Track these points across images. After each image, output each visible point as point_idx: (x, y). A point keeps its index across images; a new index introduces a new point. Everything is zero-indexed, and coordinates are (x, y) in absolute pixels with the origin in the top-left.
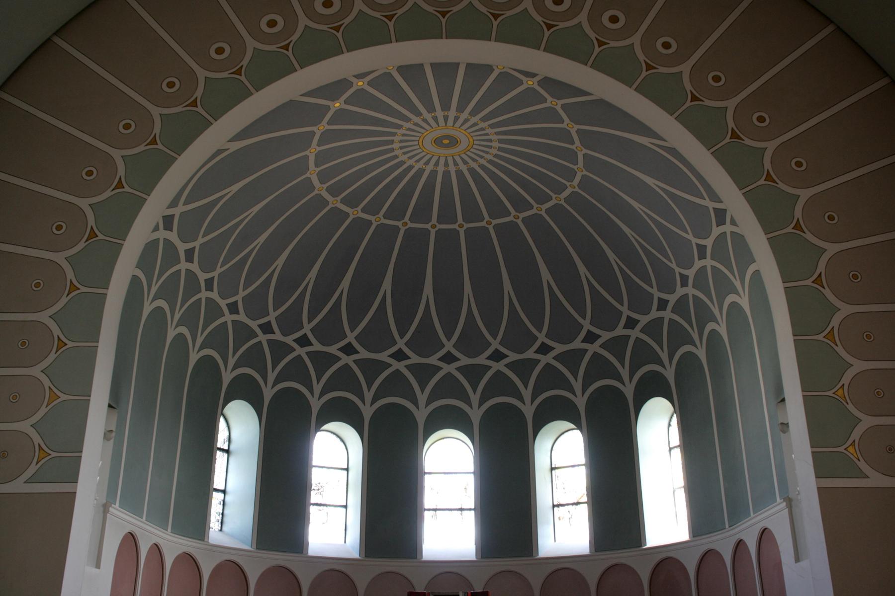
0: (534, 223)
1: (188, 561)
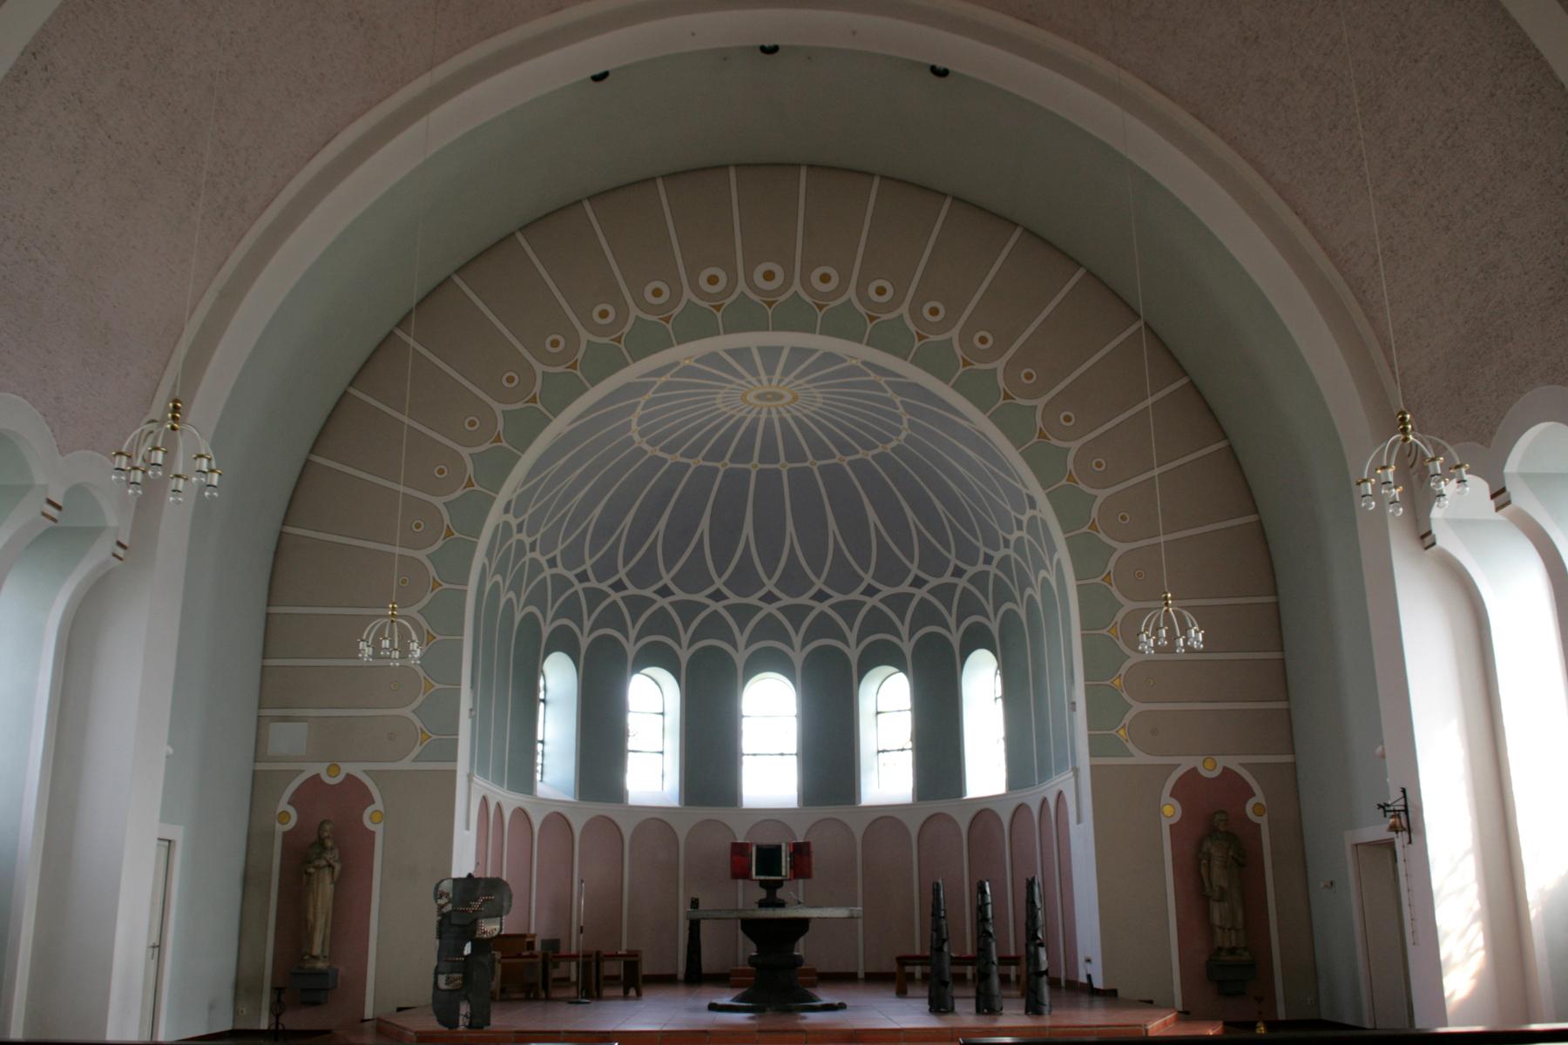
0: (858, 466)
1: (521, 814)
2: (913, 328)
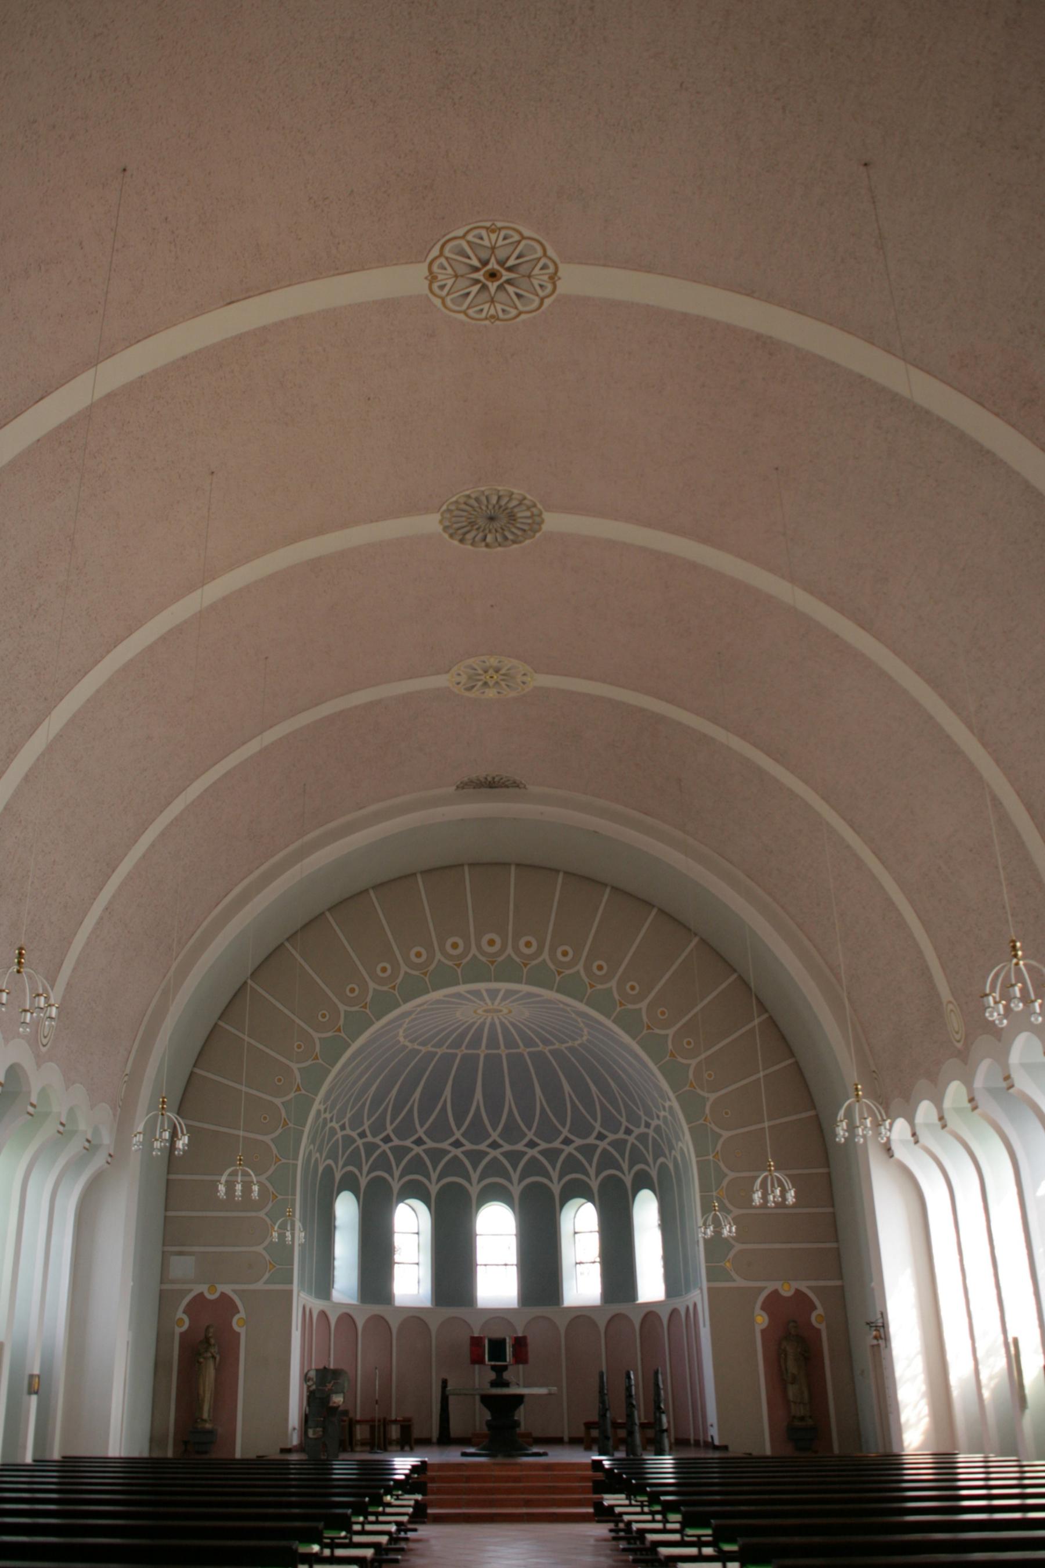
1: (323, 1314)
2: (586, 980)
